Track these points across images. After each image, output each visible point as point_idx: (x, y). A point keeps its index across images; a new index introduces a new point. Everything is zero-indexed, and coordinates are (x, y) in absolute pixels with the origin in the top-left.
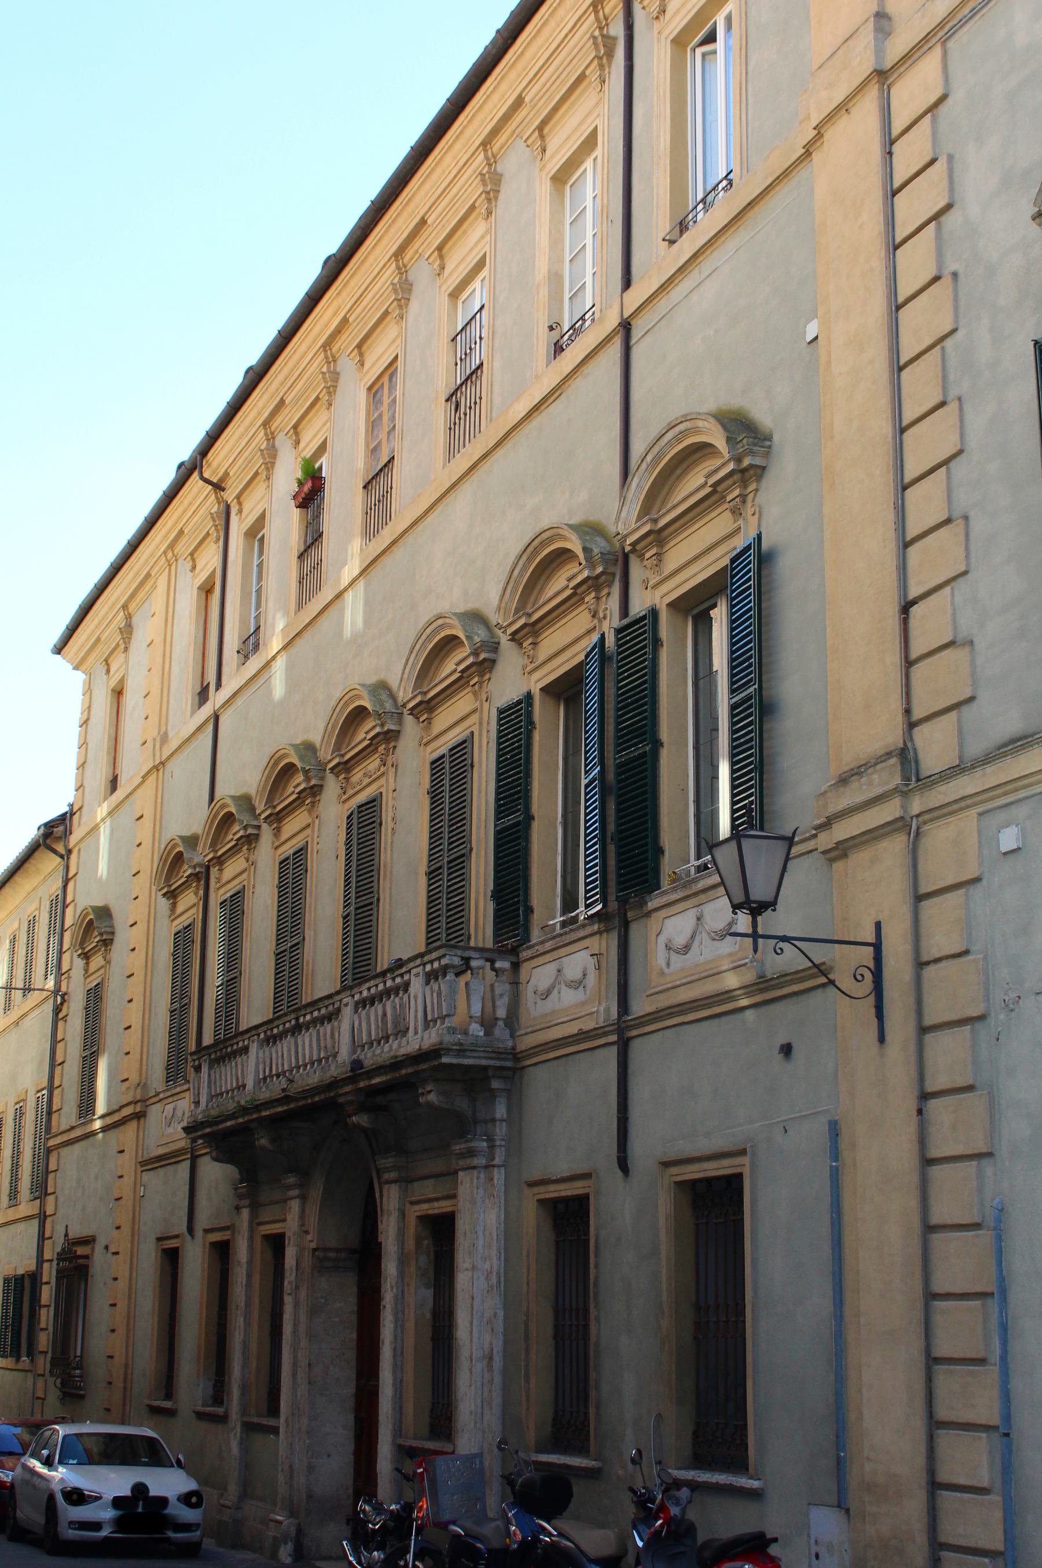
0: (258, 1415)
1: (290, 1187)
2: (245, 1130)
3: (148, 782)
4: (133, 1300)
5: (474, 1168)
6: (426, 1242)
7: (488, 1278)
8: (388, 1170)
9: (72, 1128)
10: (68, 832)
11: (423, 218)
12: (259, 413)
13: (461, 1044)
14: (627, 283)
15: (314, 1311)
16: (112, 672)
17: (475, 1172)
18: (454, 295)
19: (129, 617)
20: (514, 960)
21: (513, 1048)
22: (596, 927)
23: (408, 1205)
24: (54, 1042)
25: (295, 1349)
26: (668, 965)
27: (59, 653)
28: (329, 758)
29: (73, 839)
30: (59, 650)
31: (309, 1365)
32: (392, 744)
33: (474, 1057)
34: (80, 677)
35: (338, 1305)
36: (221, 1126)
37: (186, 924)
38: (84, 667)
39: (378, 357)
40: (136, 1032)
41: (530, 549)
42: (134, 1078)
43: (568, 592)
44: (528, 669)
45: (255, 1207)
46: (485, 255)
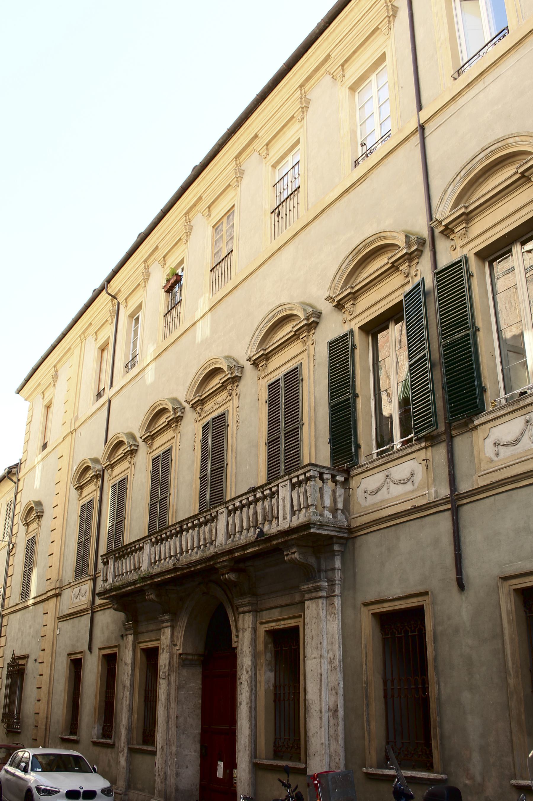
0: (138, 744)
1: (166, 621)
2: (141, 591)
3: (66, 440)
4: (52, 685)
5: (320, 597)
6: (270, 646)
7: (331, 662)
8: (243, 606)
9: (17, 604)
10: (18, 472)
11: (256, 134)
12: (142, 256)
13: (321, 522)
14: (420, 108)
15: (179, 688)
16: (45, 398)
17: (321, 601)
18: (274, 166)
19: (56, 371)
20: (346, 476)
21: (349, 525)
22: (423, 445)
23: (258, 625)
24: (8, 566)
25: (168, 708)
26: (497, 455)
27: (18, 393)
28: (192, 398)
29: (21, 475)
30: (19, 392)
31: (177, 717)
32: (236, 384)
33: (328, 530)
34: (27, 404)
35: (191, 685)
36: (123, 590)
37: (88, 501)
38: (30, 399)
39: (133, 304)
40: (56, 557)
41: (152, 408)
42: (54, 577)
43: (220, 385)
44: (199, 419)
45: (136, 634)
46: (109, 337)
